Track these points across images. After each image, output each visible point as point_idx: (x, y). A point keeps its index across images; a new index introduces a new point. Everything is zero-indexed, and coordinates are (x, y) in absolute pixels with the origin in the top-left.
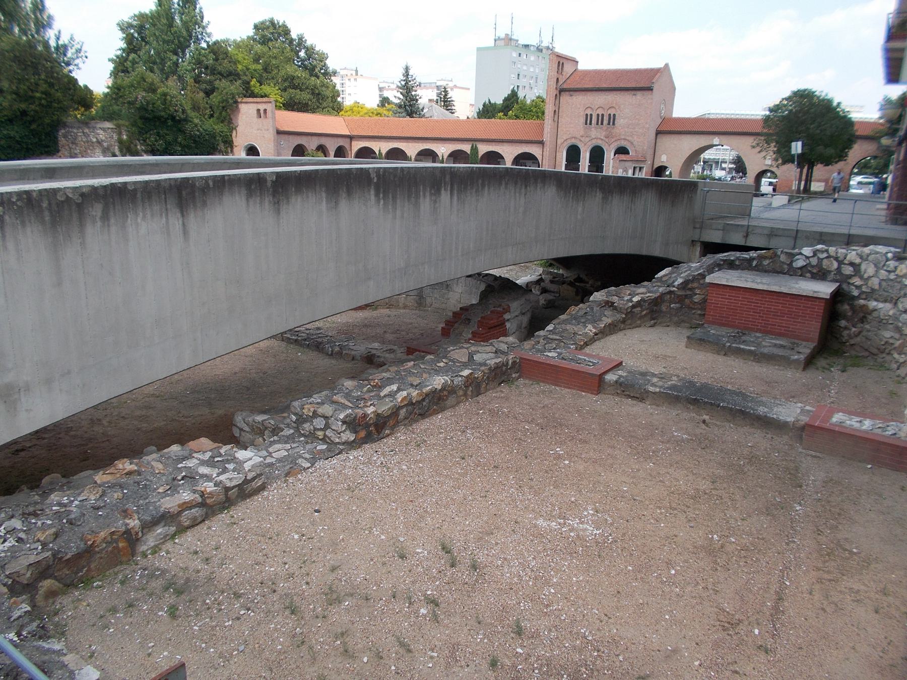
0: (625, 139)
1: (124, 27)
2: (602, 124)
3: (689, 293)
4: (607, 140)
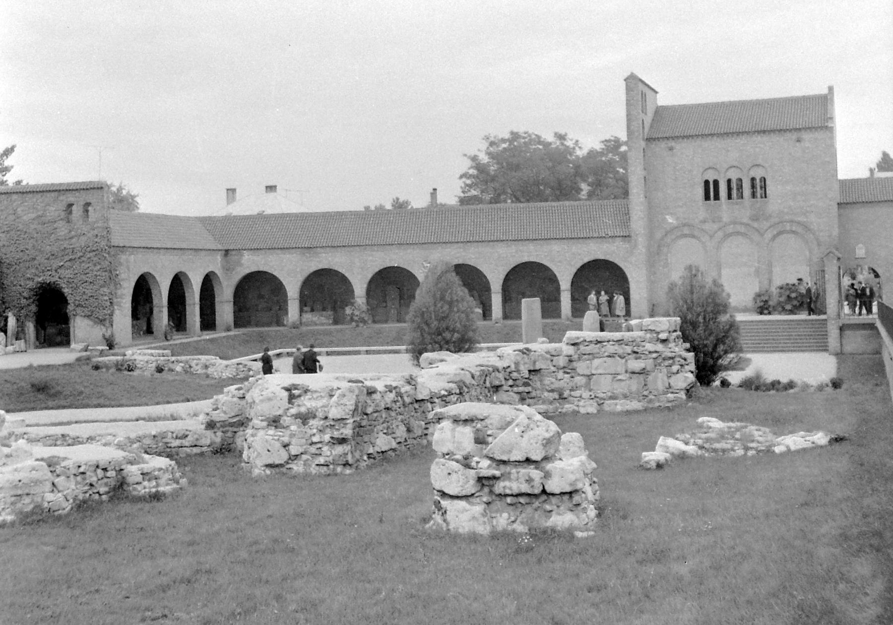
0: (792, 221)
4: (756, 225)
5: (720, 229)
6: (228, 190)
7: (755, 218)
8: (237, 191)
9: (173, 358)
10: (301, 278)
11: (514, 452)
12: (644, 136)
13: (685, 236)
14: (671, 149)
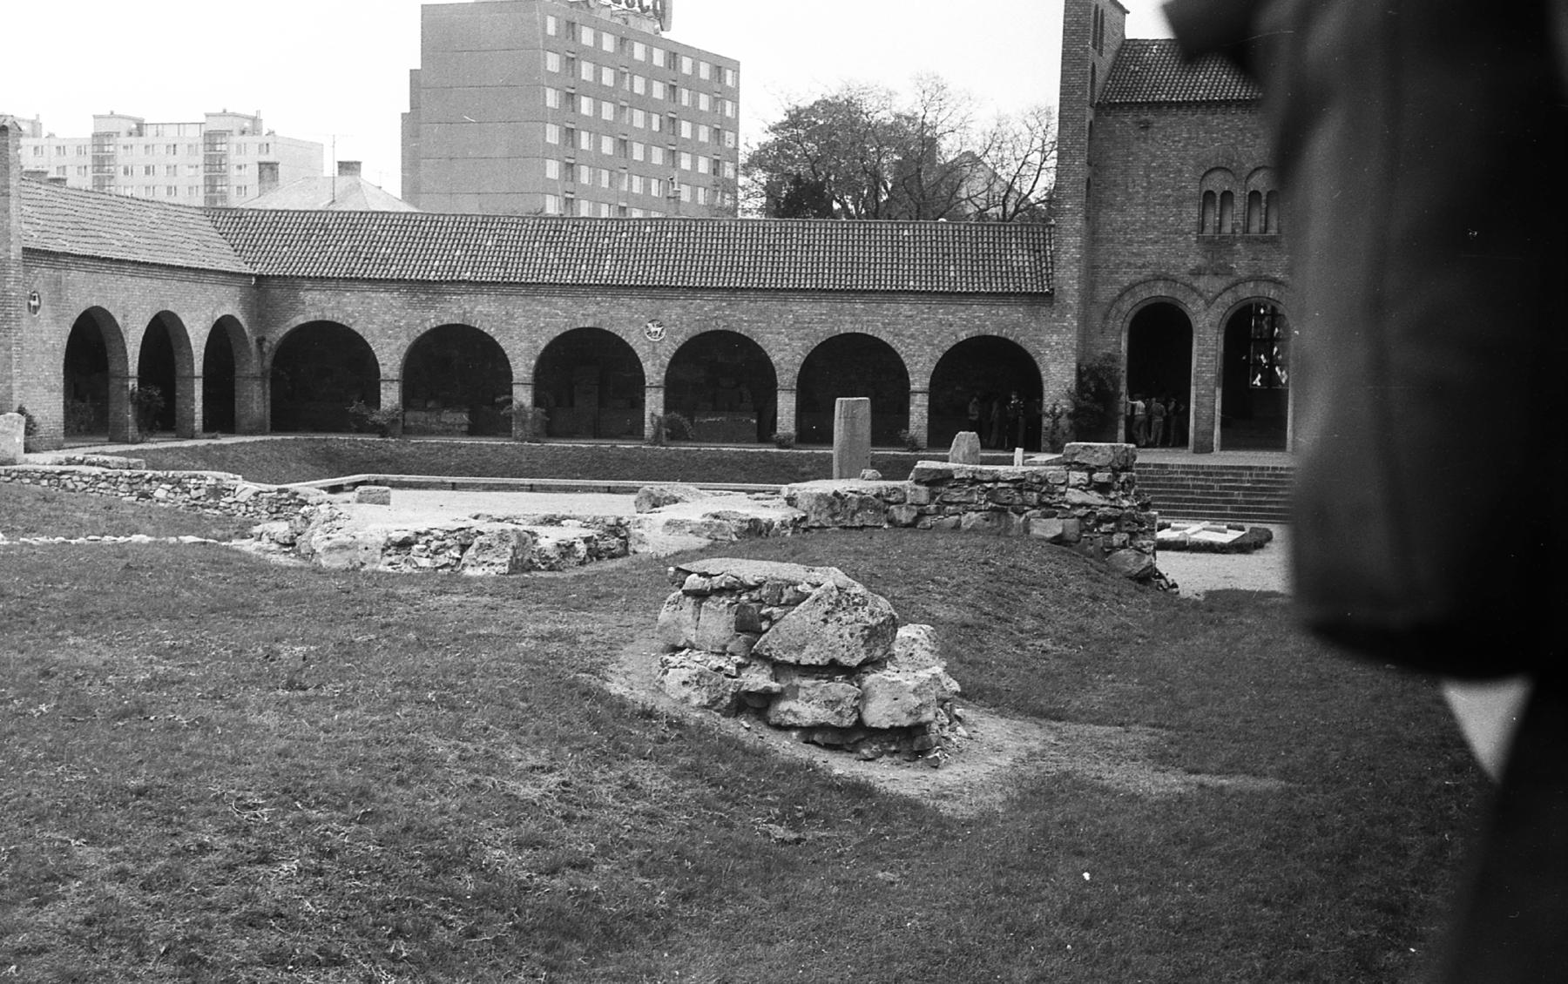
6: (260, 164)
9: (150, 474)
10: (405, 342)
11: (809, 649)
12: (1092, 97)
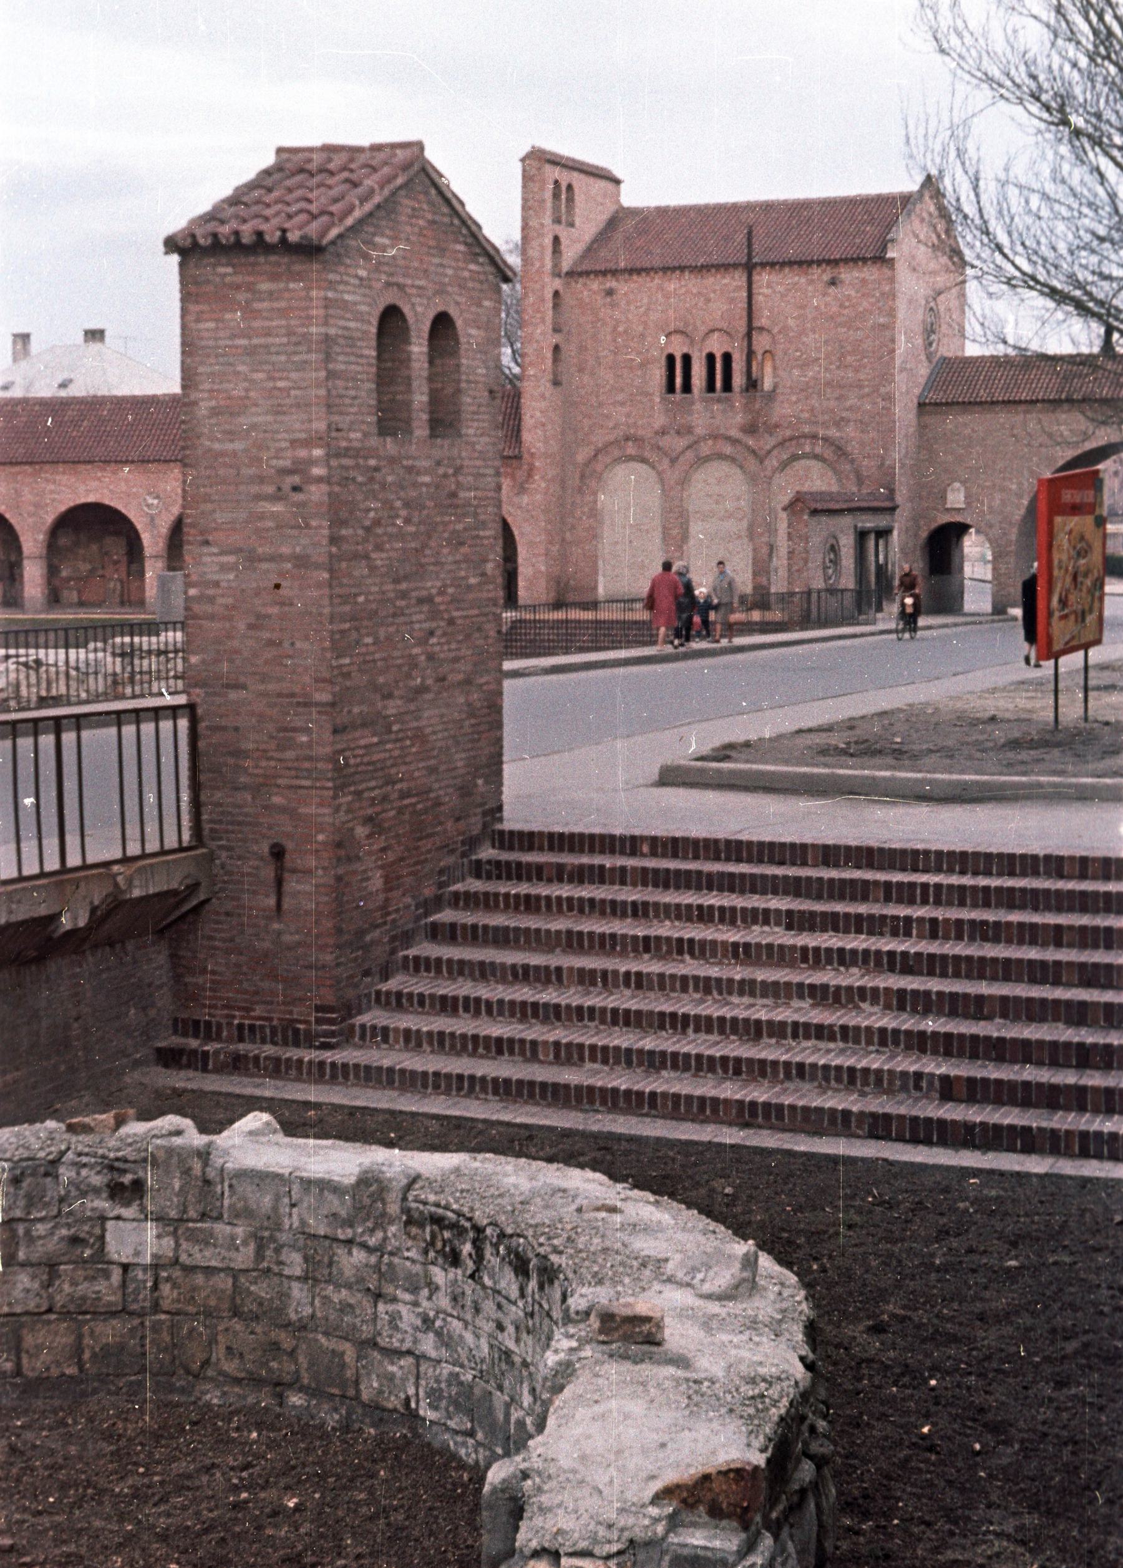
1: (280, 151)
2: (727, 387)
3: (175, 1160)
5: (689, 447)
7: (751, 429)
8: (32, 338)
13: (631, 458)
14: (610, 292)
